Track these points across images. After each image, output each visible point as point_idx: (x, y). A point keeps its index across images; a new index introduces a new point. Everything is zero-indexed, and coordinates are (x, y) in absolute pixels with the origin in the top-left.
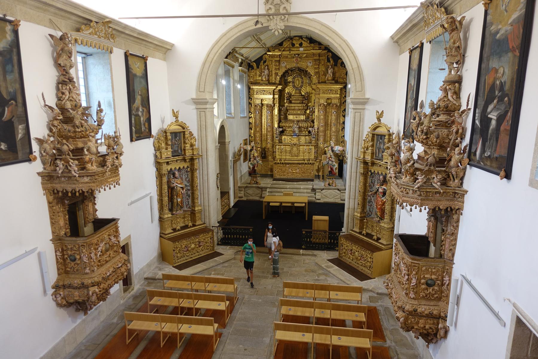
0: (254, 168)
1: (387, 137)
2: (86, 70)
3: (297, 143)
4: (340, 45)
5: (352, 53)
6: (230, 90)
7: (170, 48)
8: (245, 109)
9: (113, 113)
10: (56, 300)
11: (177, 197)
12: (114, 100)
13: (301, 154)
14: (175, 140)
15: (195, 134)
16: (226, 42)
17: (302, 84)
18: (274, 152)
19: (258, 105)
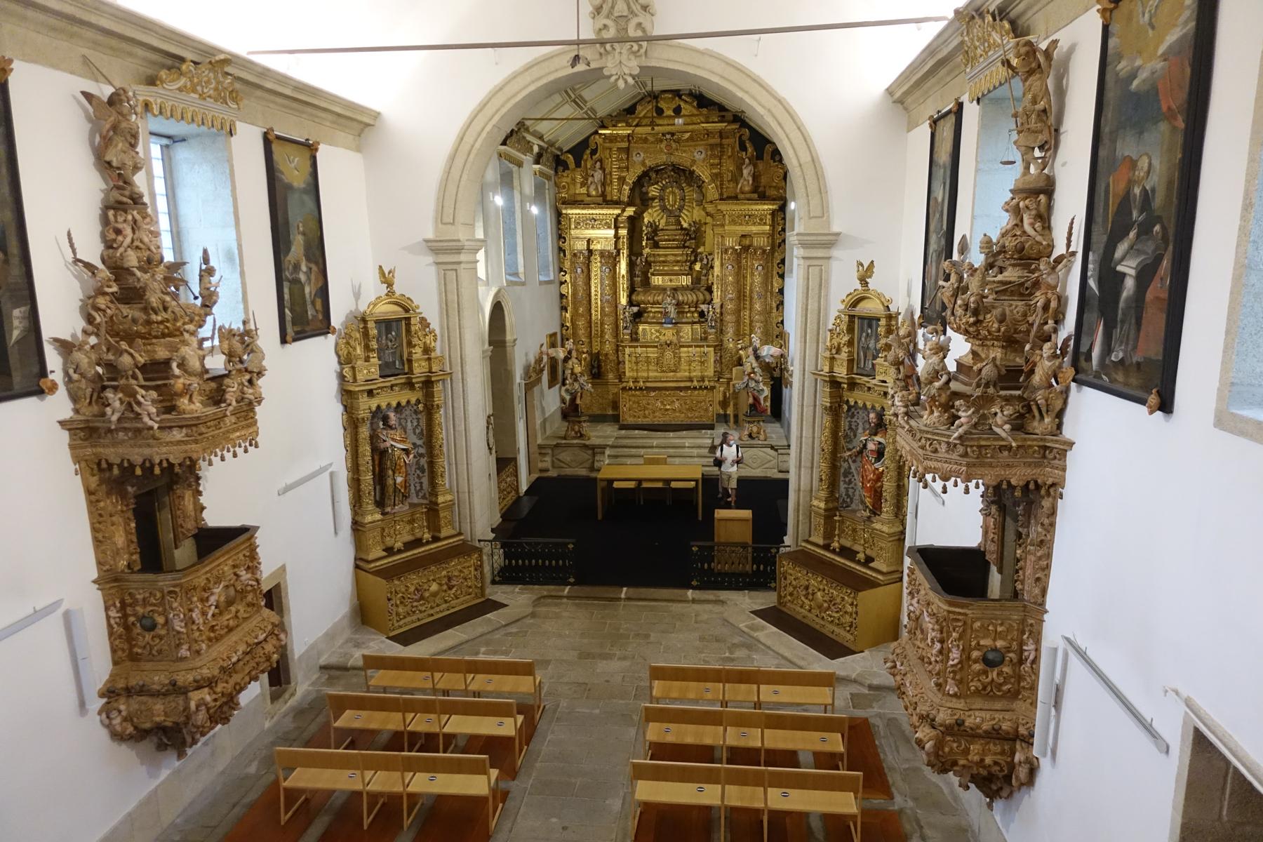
0: (573, 399)
1: (883, 322)
3: (674, 339)
4: (769, 111)
5: (799, 128)
10: (110, 724)
11: (394, 473)
13: (684, 366)
14: (387, 338)
15: (435, 325)
16: (503, 106)
18: (619, 363)
19: (581, 252)
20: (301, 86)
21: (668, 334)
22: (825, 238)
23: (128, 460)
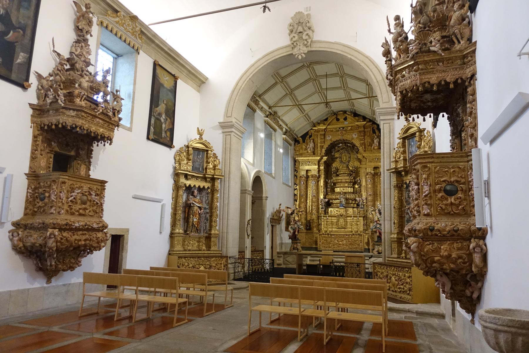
0: (294, 233)
2: (115, 69)
3: (344, 213)
4: (363, 62)
5: (376, 67)
6: (272, 152)
7: (204, 81)
8: (290, 179)
9: (131, 103)
10: (12, 239)
11: (193, 216)
12: (134, 93)
13: (349, 226)
14: (197, 157)
15: (220, 157)
16: (253, 71)
17: (349, 159)
18: (319, 225)
19: (303, 175)
20: (171, 49)
21: (342, 211)
22: (390, 110)
23: (51, 123)
